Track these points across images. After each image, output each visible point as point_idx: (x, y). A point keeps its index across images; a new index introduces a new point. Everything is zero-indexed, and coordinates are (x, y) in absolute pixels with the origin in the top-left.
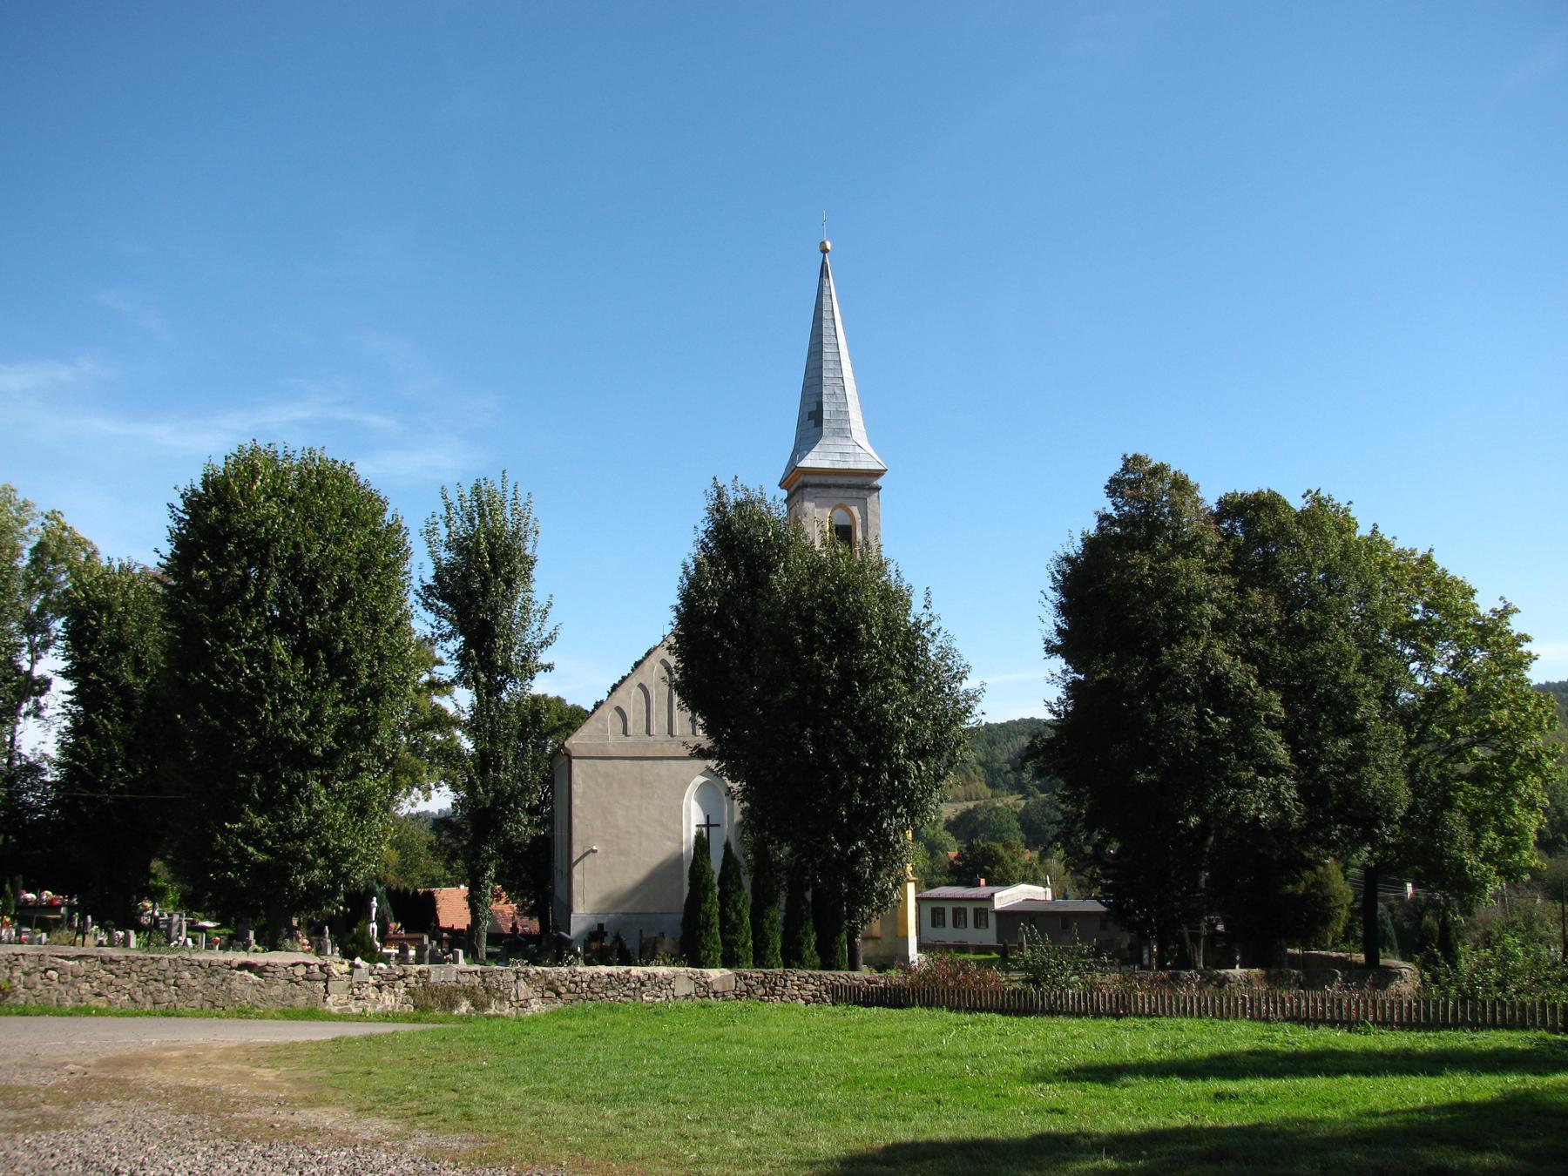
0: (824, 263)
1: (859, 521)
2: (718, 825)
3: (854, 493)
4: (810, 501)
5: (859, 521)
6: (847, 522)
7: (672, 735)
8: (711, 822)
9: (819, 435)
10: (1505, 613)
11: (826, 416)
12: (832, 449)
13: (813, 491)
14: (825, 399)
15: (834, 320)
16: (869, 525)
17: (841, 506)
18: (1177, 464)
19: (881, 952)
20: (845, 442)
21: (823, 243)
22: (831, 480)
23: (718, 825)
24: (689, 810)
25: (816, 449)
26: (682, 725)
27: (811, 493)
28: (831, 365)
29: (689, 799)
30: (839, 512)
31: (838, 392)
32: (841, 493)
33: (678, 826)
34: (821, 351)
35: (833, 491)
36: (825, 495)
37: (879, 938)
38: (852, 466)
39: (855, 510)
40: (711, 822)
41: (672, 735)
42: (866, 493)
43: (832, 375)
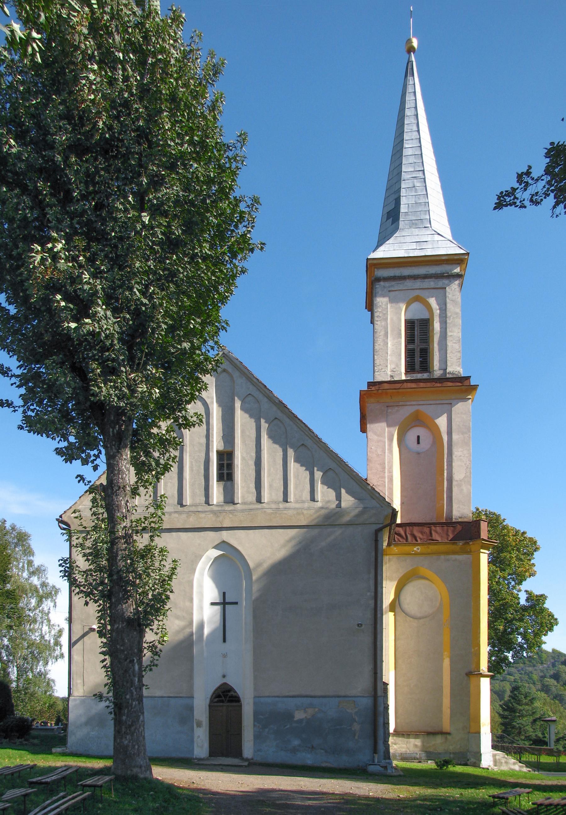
0: (409, 62)
1: (437, 312)
2: (236, 603)
3: (431, 283)
4: (384, 296)
5: (437, 312)
6: (425, 316)
7: (182, 505)
8: (227, 600)
9: (397, 229)
10: (71, 463)
11: (403, 209)
12: (408, 239)
13: (387, 284)
14: (403, 192)
15: (417, 116)
16: (449, 314)
17: (417, 299)
18: (497, 512)
19: (451, 748)
20: (424, 231)
21: (409, 41)
22: (406, 271)
23: (236, 603)
24: (201, 586)
25: (391, 241)
26: (193, 495)
27: (384, 287)
28: (412, 159)
29: (202, 574)
30: (416, 306)
31: (417, 184)
32: (418, 284)
33: (188, 604)
34: (402, 148)
35: (409, 284)
36: (401, 287)
37: (449, 734)
38: (429, 253)
39: (433, 302)
40: (227, 601)
41: (182, 505)
42: (446, 281)
43: (413, 170)
